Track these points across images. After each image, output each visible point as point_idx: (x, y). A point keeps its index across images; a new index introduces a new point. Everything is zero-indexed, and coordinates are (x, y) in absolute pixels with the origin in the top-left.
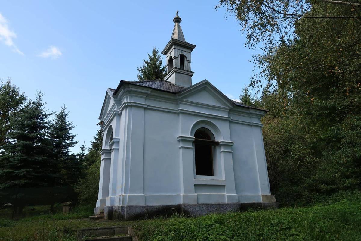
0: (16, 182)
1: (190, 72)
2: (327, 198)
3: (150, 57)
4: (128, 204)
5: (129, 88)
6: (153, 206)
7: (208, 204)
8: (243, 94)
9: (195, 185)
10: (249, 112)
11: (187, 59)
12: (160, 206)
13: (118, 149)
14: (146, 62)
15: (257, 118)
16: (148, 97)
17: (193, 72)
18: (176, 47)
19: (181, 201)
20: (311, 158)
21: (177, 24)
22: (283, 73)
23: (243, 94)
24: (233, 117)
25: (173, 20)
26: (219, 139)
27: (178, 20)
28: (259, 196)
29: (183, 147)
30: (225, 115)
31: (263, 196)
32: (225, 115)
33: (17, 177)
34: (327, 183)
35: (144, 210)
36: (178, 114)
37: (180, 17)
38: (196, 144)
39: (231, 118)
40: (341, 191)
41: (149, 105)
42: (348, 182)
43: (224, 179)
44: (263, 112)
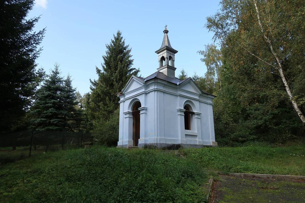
0: (51, 128)
1: (174, 67)
2: (241, 144)
3: (115, 37)
4: (159, 142)
6: (169, 144)
7: (191, 145)
8: (181, 75)
10: (207, 96)
11: (172, 59)
12: (172, 144)
13: (146, 113)
14: (113, 42)
15: (162, 86)
16: (165, 86)
17: (176, 68)
18: (168, 51)
19: (179, 142)
20: (233, 123)
21: (166, 34)
22: (296, 123)
23: (181, 75)
24: (203, 100)
25: (163, 32)
26: (195, 111)
27: (166, 32)
28: (210, 142)
29: (180, 115)
30: (197, 97)
31: (212, 142)
32: (197, 97)
33: (50, 124)
34: (242, 137)
35: (166, 146)
36: (177, 96)
37: (168, 29)
38: (185, 113)
40: (249, 141)
41: (166, 91)
42: (252, 137)
43: (196, 132)
44: (214, 97)
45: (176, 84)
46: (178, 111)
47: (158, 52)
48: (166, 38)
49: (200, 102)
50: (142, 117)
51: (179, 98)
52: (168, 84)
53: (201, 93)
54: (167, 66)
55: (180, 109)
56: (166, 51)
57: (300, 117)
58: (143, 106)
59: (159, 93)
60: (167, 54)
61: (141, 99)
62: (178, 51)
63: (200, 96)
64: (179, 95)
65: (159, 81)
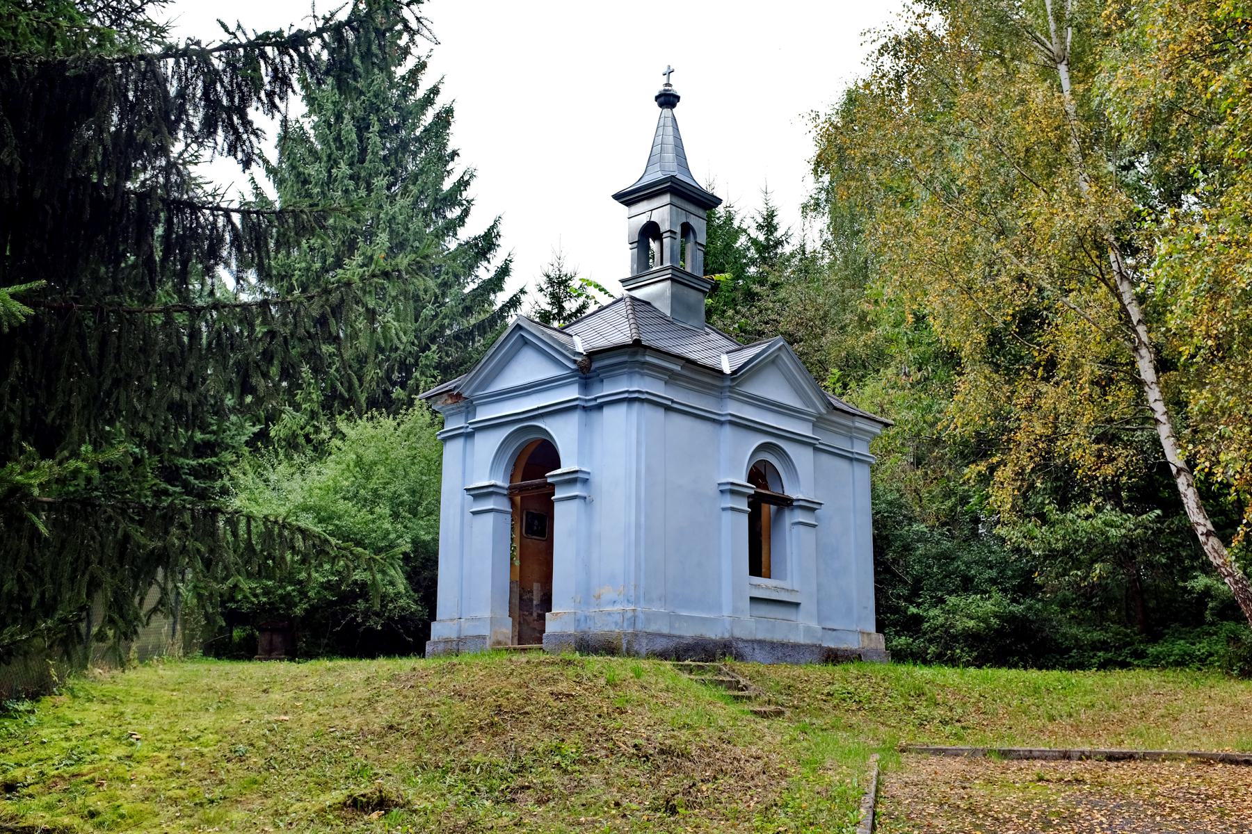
5: (644, 355)
9: (752, 599)
10: (851, 424)
11: (695, 237)
15: (660, 379)
21: (667, 112)
27: (668, 100)
29: (733, 509)
30: (804, 429)
36: (721, 423)
37: (677, 89)
38: (756, 503)
39: (817, 440)
44: (881, 426)
45: (721, 372)
46: (722, 492)
47: (628, 198)
48: (670, 130)
49: (816, 449)
50: (565, 518)
51: (727, 431)
52: (684, 372)
53: (824, 411)
54: (670, 271)
55: (732, 484)
56: (666, 199)
57: (1206, 544)
58: (568, 464)
59: (648, 410)
60: (674, 212)
61: (563, 433)
62: (678, 98)
63: (818, 422)
64: (729, 418)
65: (649, 359)
